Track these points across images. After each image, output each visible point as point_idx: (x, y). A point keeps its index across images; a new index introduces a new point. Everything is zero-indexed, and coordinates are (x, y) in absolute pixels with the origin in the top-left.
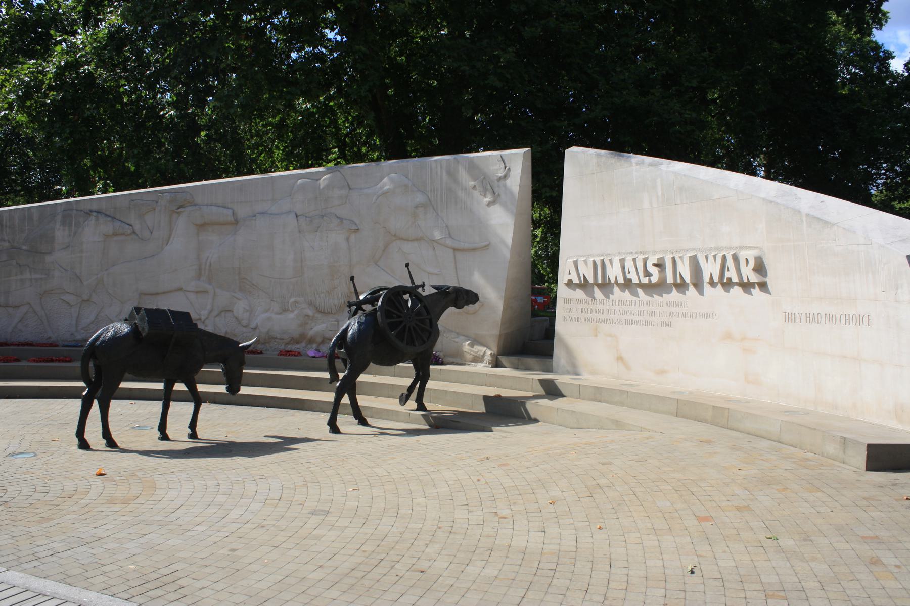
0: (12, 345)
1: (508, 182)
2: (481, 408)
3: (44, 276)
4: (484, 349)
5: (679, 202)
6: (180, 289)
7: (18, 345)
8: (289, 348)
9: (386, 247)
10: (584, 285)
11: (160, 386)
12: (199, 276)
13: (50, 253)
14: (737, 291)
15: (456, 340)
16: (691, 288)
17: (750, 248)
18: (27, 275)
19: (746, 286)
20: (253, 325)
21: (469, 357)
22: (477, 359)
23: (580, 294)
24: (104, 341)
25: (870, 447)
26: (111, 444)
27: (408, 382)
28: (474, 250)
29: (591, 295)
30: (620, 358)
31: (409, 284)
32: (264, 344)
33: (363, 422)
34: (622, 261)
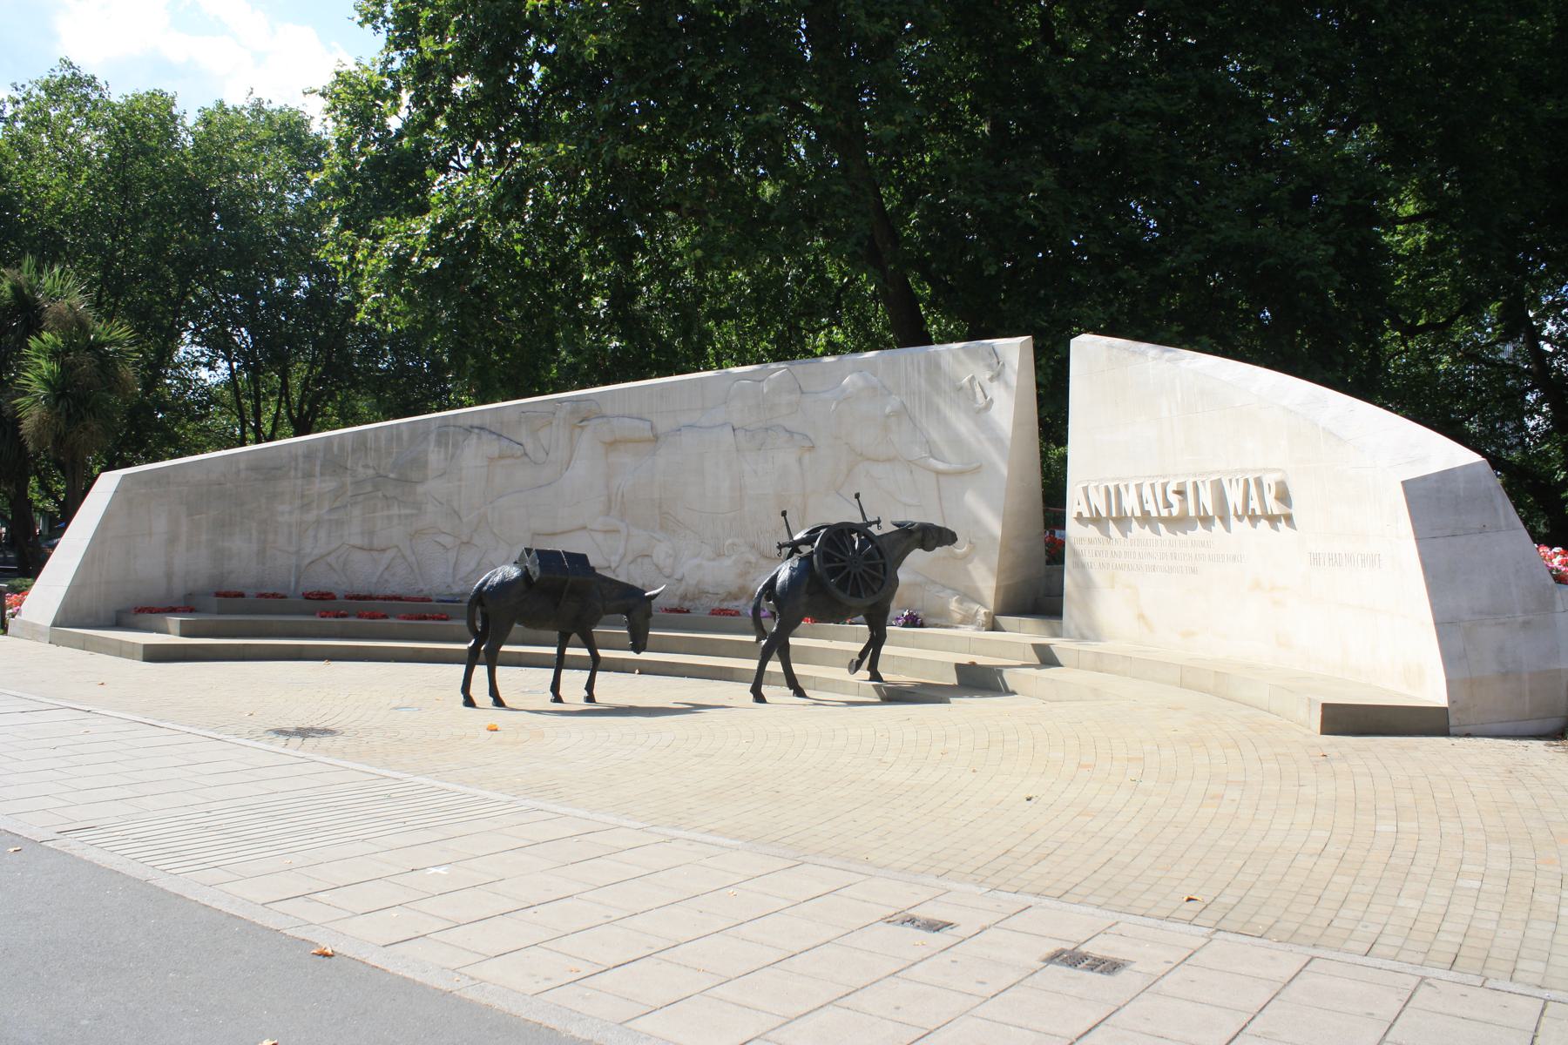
0: (377, 598)
2: (953, 680)
4: (977, 607)
6: (584, 528)
7: (385, 599)
8: (725, 605)
10: (1097, 520)
11: (553, 650)
12: (608, 511)
13: (421, 482)
14: (1264, 524)
16: (1217, 521)
17: (1274, 470)
18: (395, 511)
19: (1273, 520)
20: (678, 576)
21: (958, 617)
22: (968, 620)
23: (1092, 531)
25: (1325, 706)
26: (499, 702)
27: (860, 647)
29: (1105, 532)
30: (1141, 617)
31: (859, 520)
32: (693, 600)
33: (799, 693)
34: (1139, 487)
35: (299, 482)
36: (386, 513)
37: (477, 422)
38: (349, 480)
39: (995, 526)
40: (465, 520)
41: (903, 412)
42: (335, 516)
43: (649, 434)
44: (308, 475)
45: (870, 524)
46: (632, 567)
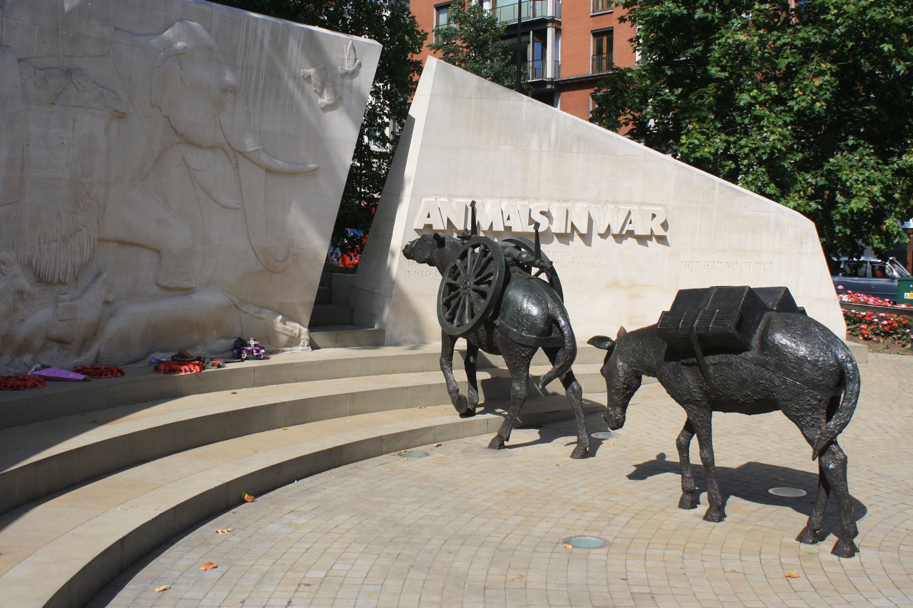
1: (356, 81)
4: (297, 325)
5: (575, 150)
21: (283, 339)
22: (293, 341)
28: (294, 174)
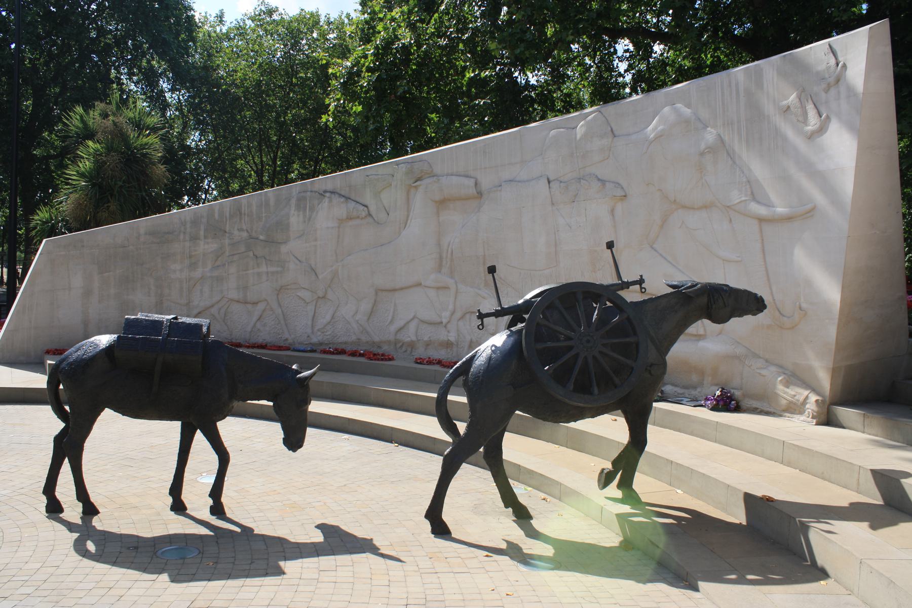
2: (737, 516)
3: (279, 269)
4: (806, 393)
6: (419, 285)
9: (664, 221)
12: (439, 268)
15: (764, 372)
18: (263, 269)
22: (795, 408)
24: (71, 364)
31: (606, 278)
35: (187, 244)
36: (256, 270)
37: (329, 187)
38: (227, 241)
39: (831, 292)
40: (320, 277)
41: (721, 147)
42: (216, 273)
43: (472, 191)
44: (194, 238)
45: (626, 285)
46: (461, 323)
